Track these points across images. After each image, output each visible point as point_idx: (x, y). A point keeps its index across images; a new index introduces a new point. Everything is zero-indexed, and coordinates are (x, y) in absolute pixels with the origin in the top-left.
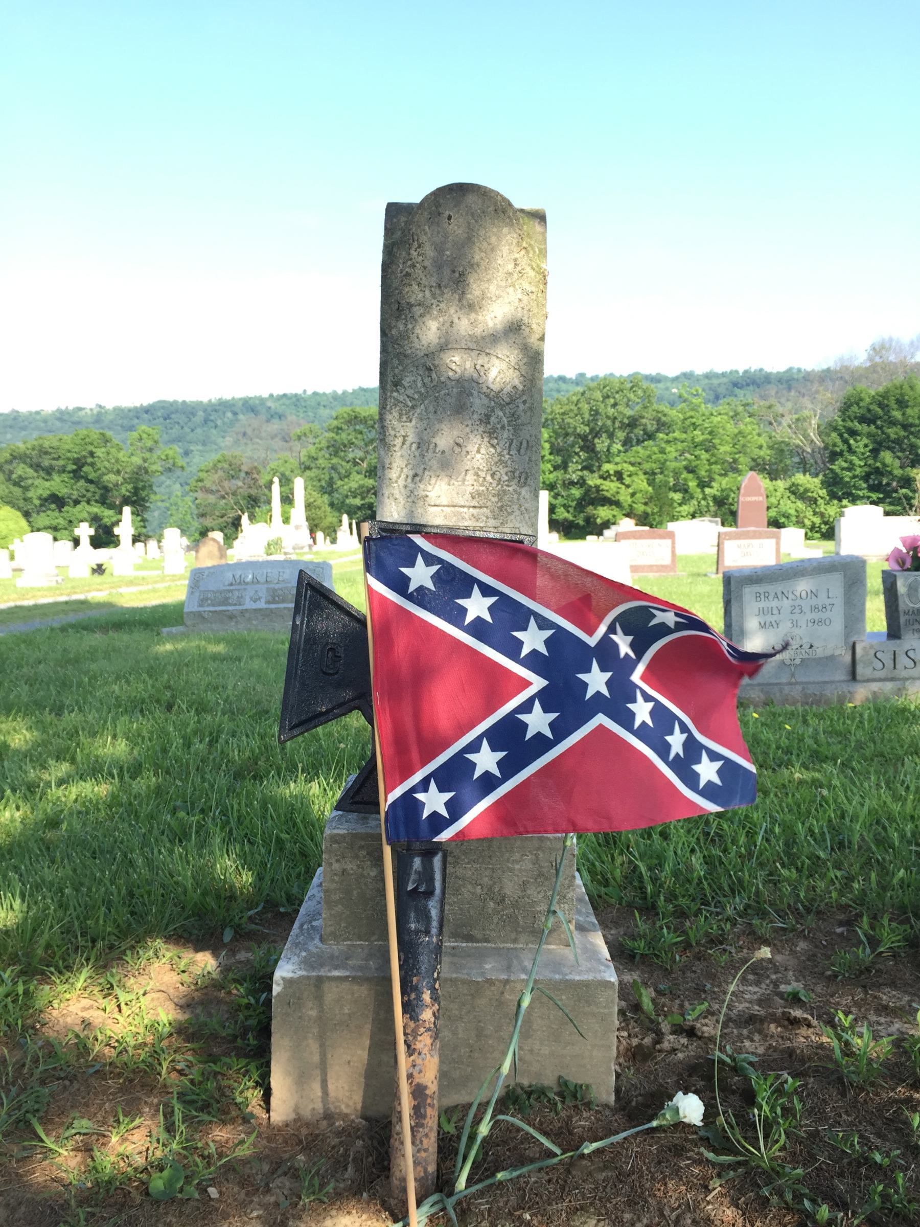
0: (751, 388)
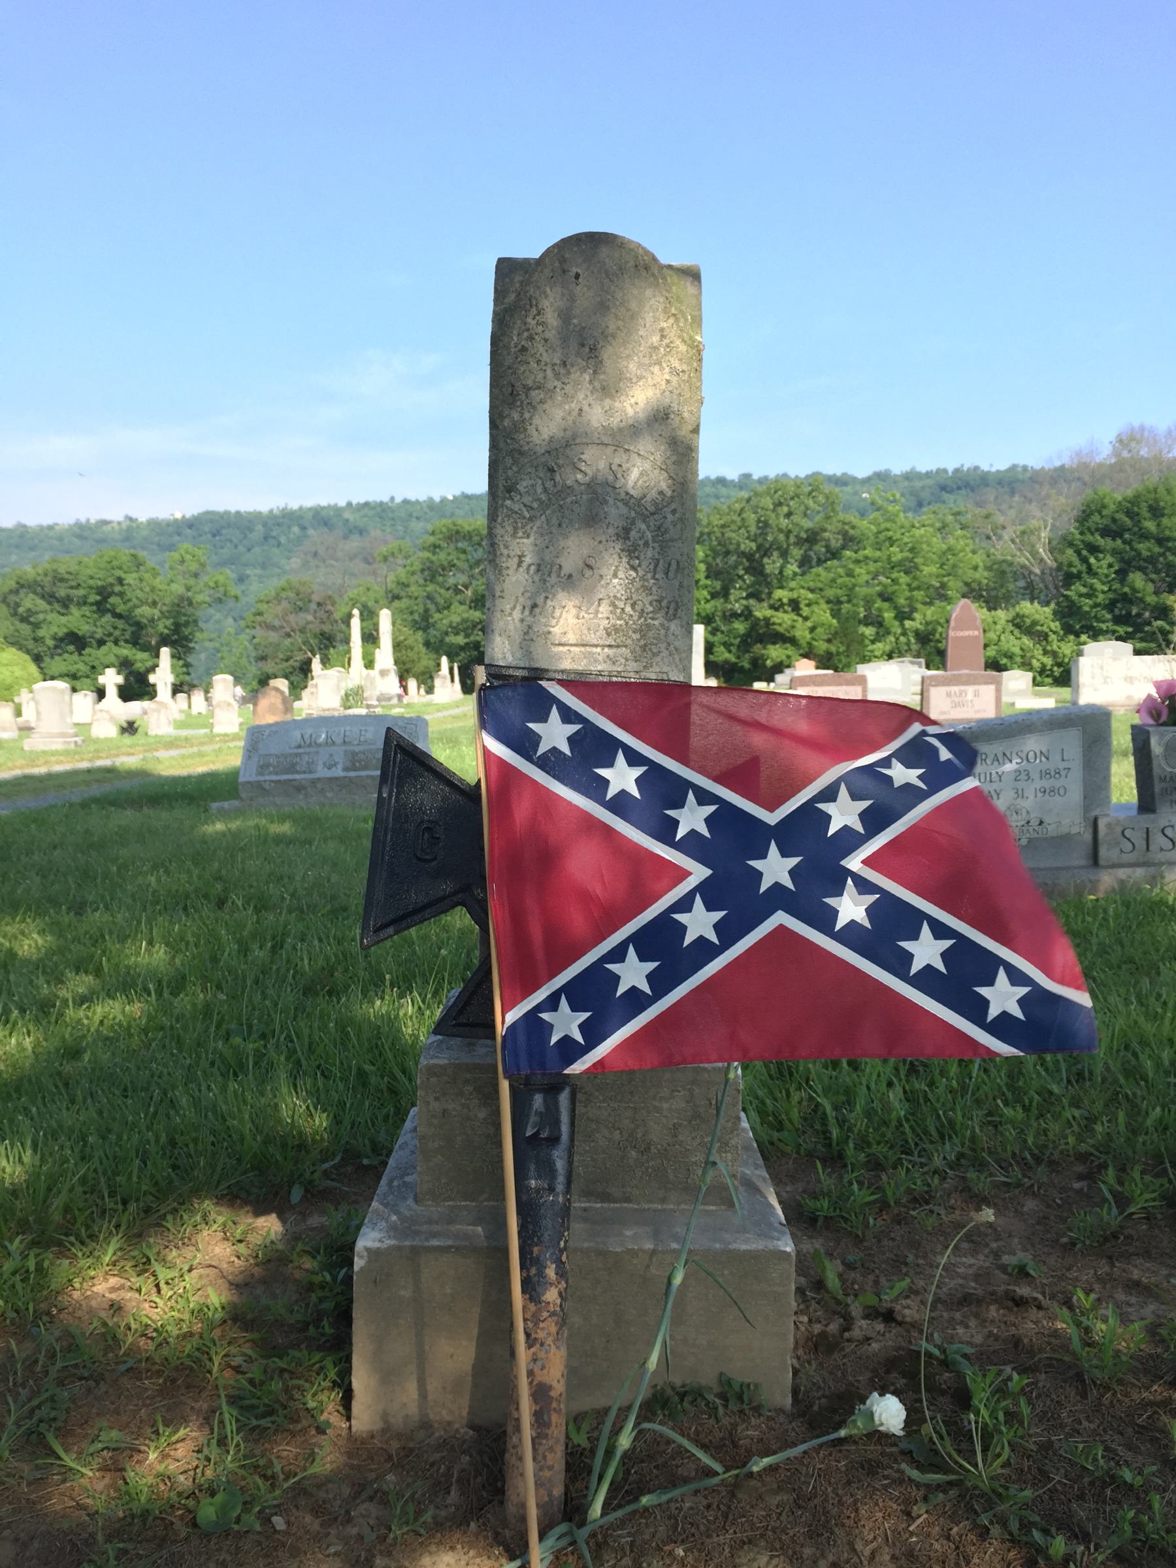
0: (963, 492)
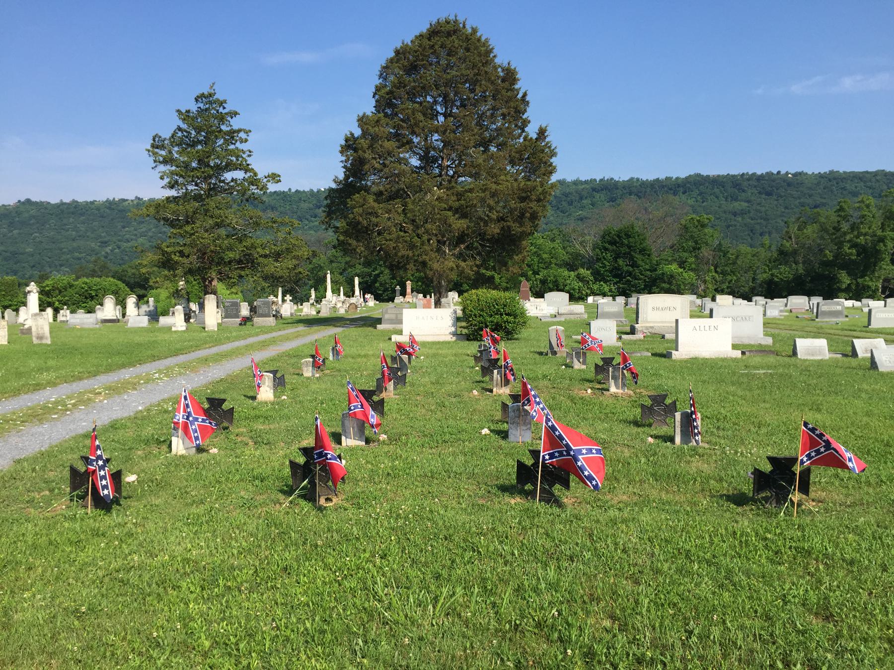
0: (604, 192)
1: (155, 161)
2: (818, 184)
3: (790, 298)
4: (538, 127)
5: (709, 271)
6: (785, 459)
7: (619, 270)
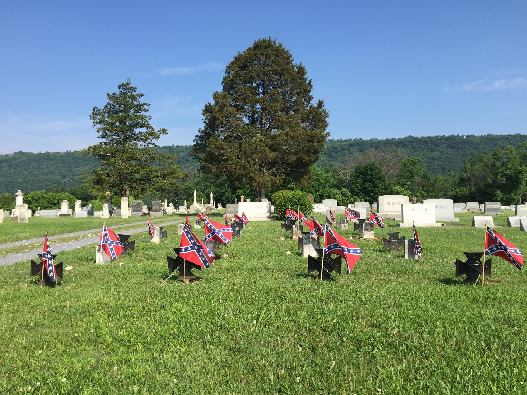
0: (356, 146)
1: (94, 123)
2: (481, 142)
3: (468, 203)
4: (318, 100)
5: (419, 190)
6: (475, 253)
7: (366, 189)
